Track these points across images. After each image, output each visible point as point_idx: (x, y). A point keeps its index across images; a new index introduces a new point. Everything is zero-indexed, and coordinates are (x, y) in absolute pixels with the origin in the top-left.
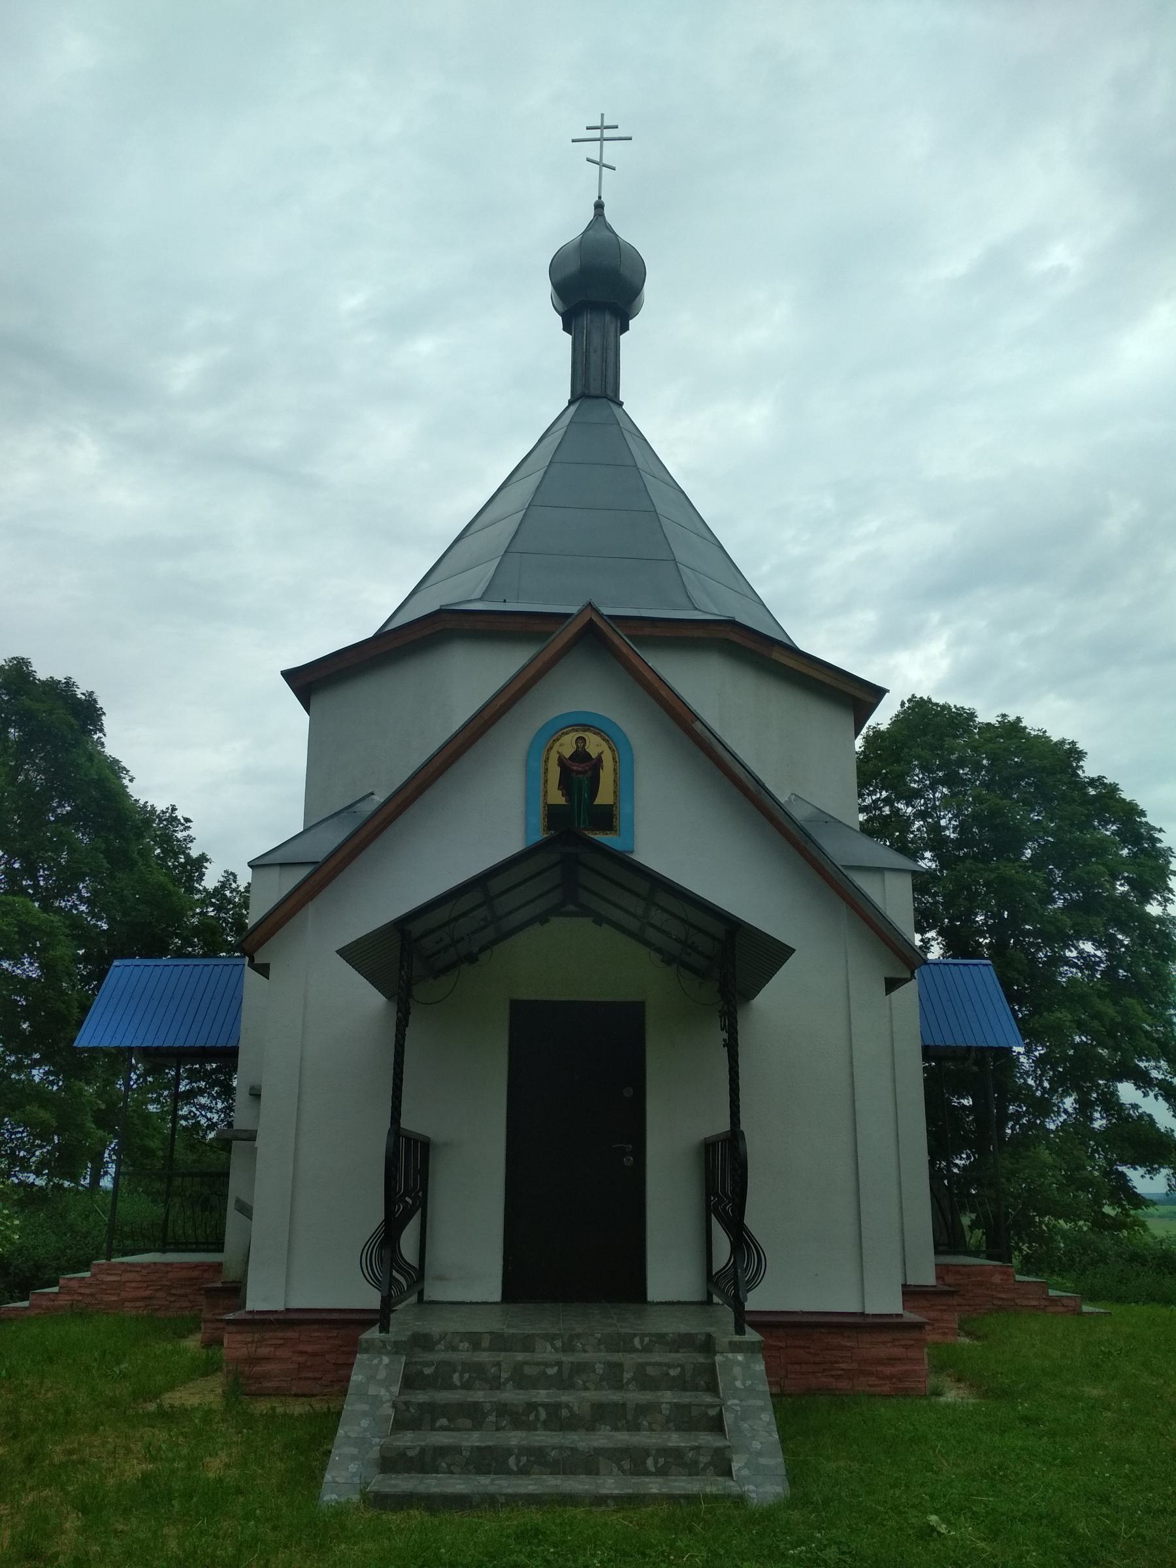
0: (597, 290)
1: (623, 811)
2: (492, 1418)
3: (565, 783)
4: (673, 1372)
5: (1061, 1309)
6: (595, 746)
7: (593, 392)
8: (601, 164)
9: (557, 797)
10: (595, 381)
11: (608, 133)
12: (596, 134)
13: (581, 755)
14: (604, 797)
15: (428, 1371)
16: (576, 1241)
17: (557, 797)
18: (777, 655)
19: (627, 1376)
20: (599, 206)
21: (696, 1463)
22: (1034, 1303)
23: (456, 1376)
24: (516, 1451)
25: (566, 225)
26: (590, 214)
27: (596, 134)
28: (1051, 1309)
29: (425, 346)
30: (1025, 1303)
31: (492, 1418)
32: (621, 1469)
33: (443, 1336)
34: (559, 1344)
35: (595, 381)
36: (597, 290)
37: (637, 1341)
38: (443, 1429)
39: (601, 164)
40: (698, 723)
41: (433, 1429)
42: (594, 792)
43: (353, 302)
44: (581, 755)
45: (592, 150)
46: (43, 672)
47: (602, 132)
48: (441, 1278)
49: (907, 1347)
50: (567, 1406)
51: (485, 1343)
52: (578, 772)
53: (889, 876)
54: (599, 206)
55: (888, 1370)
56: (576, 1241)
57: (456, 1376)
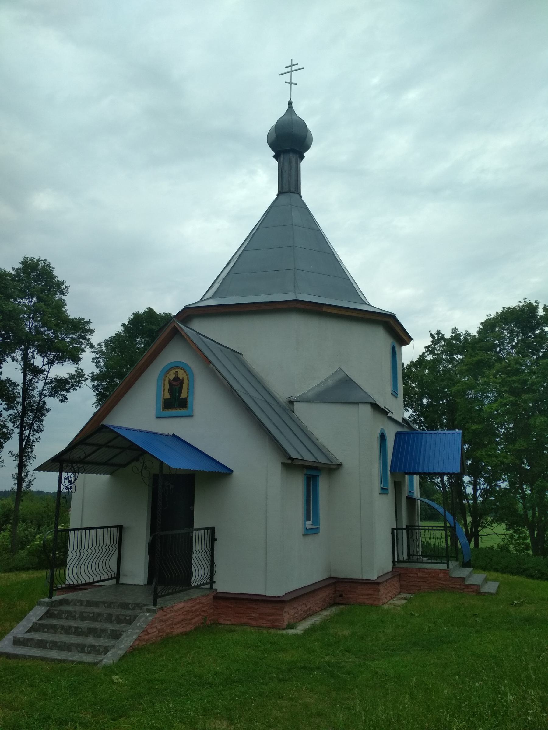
0: (289, 142)
1: (190, 400)
2: (59, 630)
3: (171, 391)
4: (127, 618)
5: (471, 590)
6: (181, 375)
7: (284, 190)
8: (291, 83)
9: (168, 396)
10: (289, 184)
11: (294, 68)
12: (289, 69)
13: (176, 379)
14: (183, 395)
15: (56, 612)
16: (170, 564)
17: (168, 396)
18: (325, 309)
19: (113, 618)
20: (290, 103)
21: (99, 650)
22: (458, 587)
23: (63, 615)
24: (36, 641)
25: (271, 116)
26: (286, 107)
27: (289, 69)
28: (466, 590)
29: (412, 95)
30: (454, 586)
31: (59, 630)
32: (77, 650)
33: (72, 600)
34: (106, 605)
35: (289, 184)
36: (289, 142)
37: (130, 606)
38: (46, 632)
39: (291, 83)
40: (211, 365)
41: (43, 632)
42: (180, 393)
43: (375, 81)
44: (176, 379)
45: (287, 77)
46: (142, 311)
47: (292, 68)
48: (125, 575)
49: (277, 609)
50: (81, 628)
51: (85, 604)
52: (175, 385)
53: (361, 406)
54: (290, 103)
55: (269, 618)
56: (170, 564)
57: (63, 615)
